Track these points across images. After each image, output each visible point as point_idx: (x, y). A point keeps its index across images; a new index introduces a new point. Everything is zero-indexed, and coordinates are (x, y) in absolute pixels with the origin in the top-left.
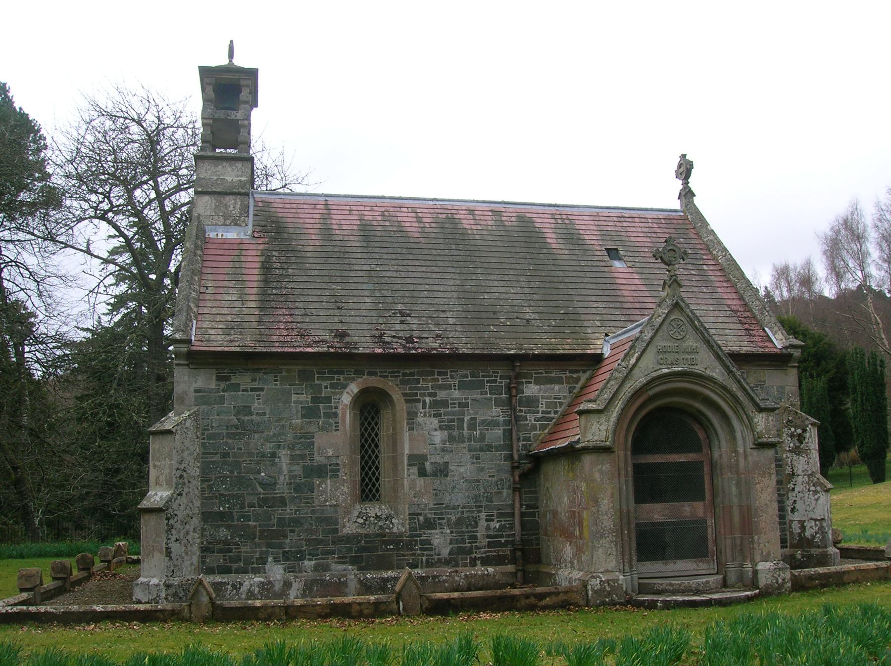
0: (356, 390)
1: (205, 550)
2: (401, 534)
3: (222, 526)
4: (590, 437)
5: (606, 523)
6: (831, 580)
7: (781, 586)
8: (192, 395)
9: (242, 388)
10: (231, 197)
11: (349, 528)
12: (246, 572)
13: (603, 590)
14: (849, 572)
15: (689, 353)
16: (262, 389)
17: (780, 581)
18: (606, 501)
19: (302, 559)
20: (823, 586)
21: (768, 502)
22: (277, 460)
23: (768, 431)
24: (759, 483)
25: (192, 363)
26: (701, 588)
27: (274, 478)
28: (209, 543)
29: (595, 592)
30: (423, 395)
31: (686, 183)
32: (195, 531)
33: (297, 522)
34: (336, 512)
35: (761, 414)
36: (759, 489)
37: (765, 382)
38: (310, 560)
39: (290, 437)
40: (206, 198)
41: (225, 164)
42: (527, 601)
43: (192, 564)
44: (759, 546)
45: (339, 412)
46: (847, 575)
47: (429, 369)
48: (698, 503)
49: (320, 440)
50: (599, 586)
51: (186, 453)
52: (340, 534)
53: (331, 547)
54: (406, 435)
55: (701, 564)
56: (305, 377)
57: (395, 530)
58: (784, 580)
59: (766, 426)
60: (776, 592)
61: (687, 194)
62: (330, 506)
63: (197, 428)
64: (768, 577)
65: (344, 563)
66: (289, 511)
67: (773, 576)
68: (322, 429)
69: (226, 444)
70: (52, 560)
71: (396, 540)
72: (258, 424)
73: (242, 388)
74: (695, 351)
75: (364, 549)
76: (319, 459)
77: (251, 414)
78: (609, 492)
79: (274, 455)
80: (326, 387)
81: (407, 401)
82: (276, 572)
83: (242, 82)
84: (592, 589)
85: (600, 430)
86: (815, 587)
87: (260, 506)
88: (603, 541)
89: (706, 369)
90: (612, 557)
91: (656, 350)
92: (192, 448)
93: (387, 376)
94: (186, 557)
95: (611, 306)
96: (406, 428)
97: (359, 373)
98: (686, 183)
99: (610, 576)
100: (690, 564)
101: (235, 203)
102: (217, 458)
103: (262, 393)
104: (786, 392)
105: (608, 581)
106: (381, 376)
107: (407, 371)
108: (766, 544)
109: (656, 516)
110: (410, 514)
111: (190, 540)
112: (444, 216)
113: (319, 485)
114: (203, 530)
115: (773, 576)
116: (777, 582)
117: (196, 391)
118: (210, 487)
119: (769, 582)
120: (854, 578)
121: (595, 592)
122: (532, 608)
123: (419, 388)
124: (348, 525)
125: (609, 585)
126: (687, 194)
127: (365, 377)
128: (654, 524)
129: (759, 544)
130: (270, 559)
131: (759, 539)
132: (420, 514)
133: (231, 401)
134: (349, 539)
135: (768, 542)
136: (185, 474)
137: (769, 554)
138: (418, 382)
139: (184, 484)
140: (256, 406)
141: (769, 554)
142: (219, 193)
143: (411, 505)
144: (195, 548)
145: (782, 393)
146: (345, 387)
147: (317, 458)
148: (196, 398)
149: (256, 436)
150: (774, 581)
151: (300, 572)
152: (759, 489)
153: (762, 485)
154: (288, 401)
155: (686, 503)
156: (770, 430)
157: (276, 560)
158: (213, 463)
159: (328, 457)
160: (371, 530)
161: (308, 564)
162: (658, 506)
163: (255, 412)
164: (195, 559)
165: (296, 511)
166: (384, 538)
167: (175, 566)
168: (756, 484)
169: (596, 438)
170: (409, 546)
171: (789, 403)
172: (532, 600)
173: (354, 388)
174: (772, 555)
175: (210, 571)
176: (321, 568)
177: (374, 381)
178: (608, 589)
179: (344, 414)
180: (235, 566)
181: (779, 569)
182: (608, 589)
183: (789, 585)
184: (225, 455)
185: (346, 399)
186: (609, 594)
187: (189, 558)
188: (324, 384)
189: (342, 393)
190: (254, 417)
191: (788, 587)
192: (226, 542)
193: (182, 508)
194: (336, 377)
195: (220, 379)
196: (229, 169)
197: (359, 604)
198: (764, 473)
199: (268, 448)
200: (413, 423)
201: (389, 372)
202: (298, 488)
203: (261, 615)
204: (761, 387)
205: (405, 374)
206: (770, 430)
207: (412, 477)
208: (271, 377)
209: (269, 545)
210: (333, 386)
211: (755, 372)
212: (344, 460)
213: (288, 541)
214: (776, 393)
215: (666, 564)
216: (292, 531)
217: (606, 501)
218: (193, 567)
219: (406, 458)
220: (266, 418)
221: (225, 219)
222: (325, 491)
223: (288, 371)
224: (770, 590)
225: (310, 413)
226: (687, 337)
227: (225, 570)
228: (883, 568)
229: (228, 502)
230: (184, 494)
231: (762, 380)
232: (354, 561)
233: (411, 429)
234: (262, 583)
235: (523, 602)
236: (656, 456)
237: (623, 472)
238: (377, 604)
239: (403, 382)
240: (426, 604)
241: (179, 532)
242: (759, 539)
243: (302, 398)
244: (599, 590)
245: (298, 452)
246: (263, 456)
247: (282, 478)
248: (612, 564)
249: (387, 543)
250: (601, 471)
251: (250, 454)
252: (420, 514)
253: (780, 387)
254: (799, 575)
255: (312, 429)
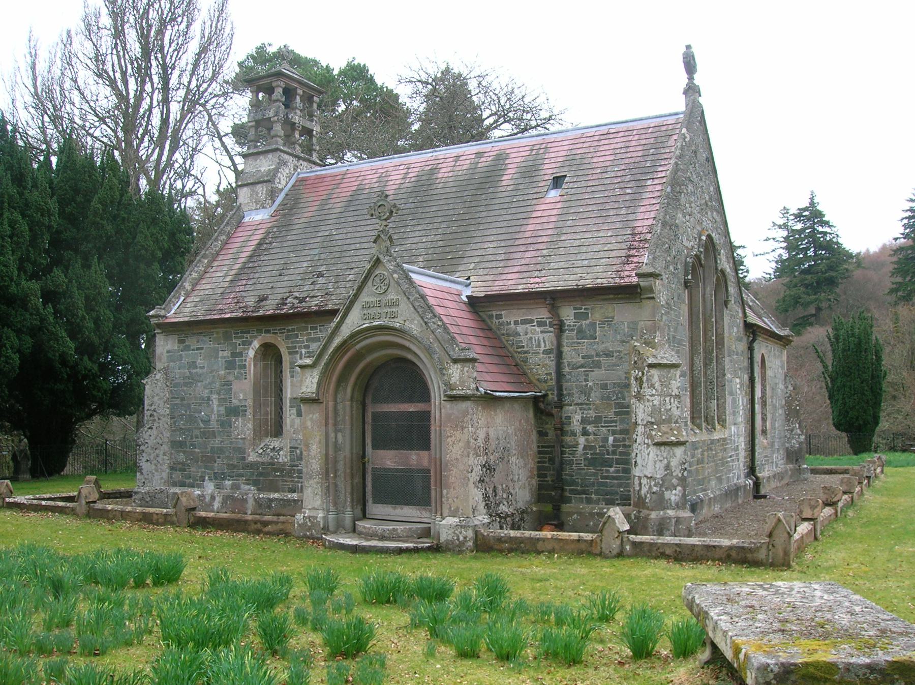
0: (257, 346)
1: (172, 468)
2: (284, 464)
3: (181, 451)
4: (304, 389)
5: (314, 467)
6: (522, 545)
7: (462, 544)
8: (165, 354)
9: (192, 348)
10: (260, 185)
11: (252, 457)
12: (193, 486)
13: (305, 524)
14: (544, 540)
15: (389, 306)
16: (202, 348)
17: (461, 538)
18: (314, 447)
19: (224, 479)
20: (511, 550)
21: (459, 457)
22: (211, 402)
23: (462, 382)
24: (451, 437)
25: (165, 332)
26: (386, 535)
27: (208, 416)
28: (174, 464)
29: (299, 525)
30: (300, 347)
31: (691, 78)
32: (164, 454)
33: (221, 450)
34: (244, 444)
35: (456, 366)
36: (451, 443)
37: (613, 318)
38: (229, 480)
39: (217, 385)
40: (245, 189)
41: (261, 157)
42: (256, 526)
43: (162, 478)
44: (448, 500)
45: (247, 364)
46: (541, 542)
47: (304, 325)
48: (424, 452)
49: (235, 387)
50: (302, 521)
51: (156, 398)
52: (247, 461)
53: (241, 471)
54: (289, 381)
55: (424, 512)
56: (227, 337)
57: (281, 460)
58: (465, 538)
59: (460, 378)
60: (457, 549)
61: (692, 90)
62: (241, 439)
63: (167, 379)
64: (450, 532)
65: (248, 484)
66: (216, 442)
67: (454, 533)
68: (237, 378)
69: (183, 391)
70: (841, 476)
71: (281, 468)
72: (200, 375)
73: (192, 348)
74: (395, 304)
75: (261, 474)
76: (235, 402)
77: (196, 367)
78: (317, 439)
79: (209, 399)
80: (239, 345)
81: (290, 353)
82: (210, 487)
83: (274, 84)
84: (298, 523)
85: (312, 383)
86: (501, 551)
87: (202, 438)
88: (311, 482)
89: (405, 321)
90: (318, 497)
91: (361, 306)
92: (162, 394)
93: (277, 333)
94: (156, 473)
95: (502, 245)
96: (289, 375)
97: (260, 331)
98: (691, 78)
99: (313, 513)
100: (414, 511)
101: (263, 190)
102: (178, 401)
103: (202, 351)
104: (639, 328)
105: (309, 517)
106: (273, 333)
107: (290, 328)
108: (455, 500)
109: (388, 463)
110: (291, 448)
111: (160, 460)
112: (468, 162)
113: (235, 423)
114: (172, 454)
115: (454, 533)
116: (458, 539)
117: (168, 352)
118: (175, 422)
119: (450, 538)
120: (549, 547)
121: (299, 525)
122: (258, 532)
123: (298, 342)
124: (251, 454)
125: (310, 520)
126: (692, 90)
127: (263, 334)
128: (385, 469)
129: (448, 498)
130: (207, 478)
131: (448, 493)
132: (297, 448)
133: (186, 359)
134: (252, 465)
135: (457, 498)
136: (155, 414)
137: (457, 509)
138: (297, 336)
139: (155, 420)
140: (199, 361)
141: (457, 509)
142: (252, 184)
143: (292, 439)
144: (165, 467)
145: (635, 329)
146: (250, 343)
147: (234, 401)
148: (168, 357)
149: (199, 384)
150: (455, 538)
151: (223, 489)
152: (451, 443)
153: (453, 438)
154: (217, 357)
155: (414, 452)
156: (464, 382)
157: (210, 479)
158: (176, 404)
159: (240, 400)
160: (266, 459)
161: (228, 483)
162: (391, 453)
163: (198, 366)
164: (165, 475)
165: (222, 441)
166: (273, 466)
167: (146, 479)
168: (448, 437)
169: (308, 390)
170: (290, 473)
171: (643, 341)
172: (259, 526)
173: (256, 344)
174: (461, 511)
175: (175, 484)
176: (235, 487)
177: (268, 338)
178: (309, 524)
179: (250, 365)
180: (187, 481)
181: (461, 527)
182: (309, 524)
183: (471, 543)
184: (183, 399)
185: (251, 353)
186: (310, 529)
187: (158, 474)
188: (238, 342)
189: (249, 348)
190: (198, 370)
191: (470, 546)
192: (183, 464)
193: (152, 438)
194: (245, 335)
195: (181, 342)
196: (264, 161)
197: (157, 514)
198: (457, 426)
199: (206, 393)
200: (293, 372)
201: (279, 330)
202: (222, 424)
203: (111, 516)
204: (608, 324)
205: (289, 331)
206: (464, 382)
207: (293, 417)
208: (207, 339)
209: (206, 467)
210: (244, 343)
211: (601, 308)
212: (250, 402)
213: (216, 465)
214: (626, 330)
215: (395, 508)
216: (219, 457)
217: (314, 447)
218: (163, 481)
219: (288, 401)
220: (205, 370)
221: (257, 204)
222: (237, 427)
223: (217, 333)
224: (451, 547)
225: (230, 365)
226: (390, 290)
227: (182, 485)
228: (586, 541)
229: (184, 434)
230: (154, 428)
231: (610, 315)
232: (255, 483)
233: (292, 377)
234: (199, 495)
235: (253, 527)
236: (390, 405)
237: (331, 421)
238: (166, 515)
239: (287, 338)
240: (192, 520)
241: (150, 454)
242: (448, 493)
243: (225, 354)
244: (303, 524)
245: (222, 396)
246: (203, 400)
247: (213, 416)
248: (318, 503)
249: (276, 470)
250: (311, 419)
251: (196, 398)
252: (297, 448)
253: (632, 322)
254: (488, 535)
255: (231, 378)
